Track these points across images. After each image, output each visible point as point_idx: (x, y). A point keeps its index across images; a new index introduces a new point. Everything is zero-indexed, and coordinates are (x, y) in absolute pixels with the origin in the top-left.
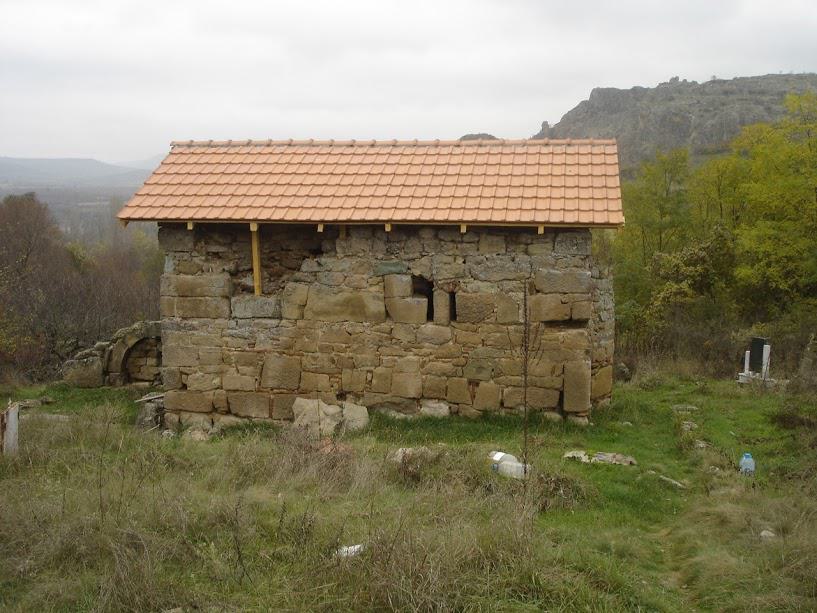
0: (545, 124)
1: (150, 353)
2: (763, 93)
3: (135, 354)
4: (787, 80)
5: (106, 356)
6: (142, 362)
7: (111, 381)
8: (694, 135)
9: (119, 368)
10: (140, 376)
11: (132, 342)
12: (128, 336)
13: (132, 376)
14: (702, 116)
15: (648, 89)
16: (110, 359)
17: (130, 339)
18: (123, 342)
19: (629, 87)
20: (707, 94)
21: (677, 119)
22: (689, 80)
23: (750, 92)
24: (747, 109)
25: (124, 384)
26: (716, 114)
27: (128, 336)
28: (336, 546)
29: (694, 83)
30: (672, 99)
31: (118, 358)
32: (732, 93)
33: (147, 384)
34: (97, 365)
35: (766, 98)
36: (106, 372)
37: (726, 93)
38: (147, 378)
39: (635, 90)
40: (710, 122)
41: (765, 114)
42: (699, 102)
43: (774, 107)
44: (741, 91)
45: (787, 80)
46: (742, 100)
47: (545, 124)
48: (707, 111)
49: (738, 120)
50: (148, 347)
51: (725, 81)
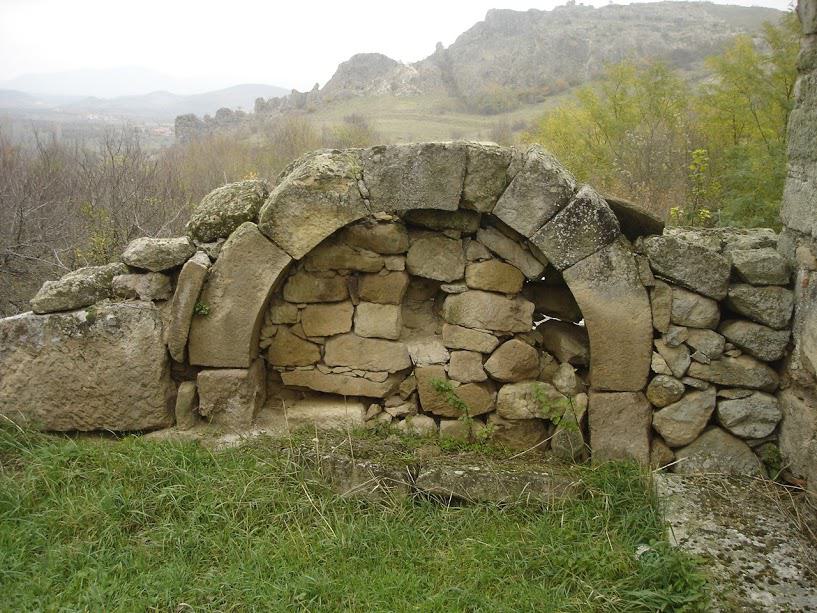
0: (439, 45)
1: (367, 285)
2: (659, 19)
3: (302, 288)
4: (683, 8)
5: (186, 293)
6: (335, 319)
7: (205, 406)
8: (591, 60)
9: (242, 350)
10: (323, 381)
11: (303, 237)
12: (295, 208)
13: (288, 379)
14: (599, 41)
15: (544, 12)
16: (198, 315)
17: (300, 221)
18: (268, 235)
19: (526, 10)
20: (604, 19)
21: (575, 43)
22: (586, 4)
23: (647, 18)
24: (643, 35)
25: (256, 419)
26: (612, 40)
27: (295, 208)
28: (112, 278)
29: (591, 7)
30: (569, 22)
31: (235, 306)
32: (628, 18)
33: (355, 411)
34: (140, 335)
35: (662, 25)
36: (180, 367)
37: (623, 18)
38: (356, 387)
39: (531, 12)
40: (608, 47)
41: (662, 40)
42: (595, 27)
43: (671, 34)
44: (638, 17)
45: (683, 8)
46: (639, 25)
47: (439, 45)
48: (604, 35)
49: (636, 46)
50: (368, 259)
51: (621, 7)
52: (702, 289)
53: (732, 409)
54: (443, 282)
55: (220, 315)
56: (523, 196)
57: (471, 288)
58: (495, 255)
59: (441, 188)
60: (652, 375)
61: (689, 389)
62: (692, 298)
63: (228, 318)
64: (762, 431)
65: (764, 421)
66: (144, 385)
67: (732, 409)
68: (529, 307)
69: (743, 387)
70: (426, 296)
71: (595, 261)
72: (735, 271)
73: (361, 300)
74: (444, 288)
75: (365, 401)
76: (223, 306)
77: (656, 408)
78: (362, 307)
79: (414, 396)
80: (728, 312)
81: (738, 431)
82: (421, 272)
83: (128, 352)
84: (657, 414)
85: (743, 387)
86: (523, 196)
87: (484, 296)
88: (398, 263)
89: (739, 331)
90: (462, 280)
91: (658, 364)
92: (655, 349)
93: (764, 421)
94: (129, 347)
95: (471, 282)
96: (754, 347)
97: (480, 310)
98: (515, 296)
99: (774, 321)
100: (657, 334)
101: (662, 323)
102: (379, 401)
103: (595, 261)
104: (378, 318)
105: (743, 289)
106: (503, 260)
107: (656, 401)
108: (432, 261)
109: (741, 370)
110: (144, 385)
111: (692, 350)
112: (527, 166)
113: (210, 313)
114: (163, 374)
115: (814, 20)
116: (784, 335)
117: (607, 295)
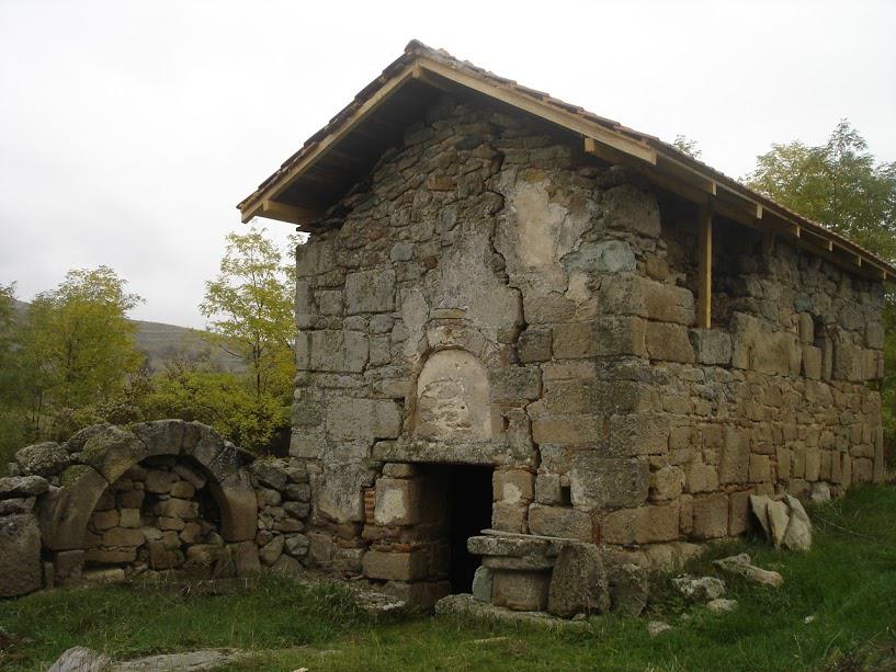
10: (105, 557)
12: (114, 456)
17: (115, 462)
33: (119, 572)
38: (121, 557)
52: (277, 487)
53: (291, 542)
54: (162, 494)
55: (70, 519)
56: (206, 446)
57: (172, 497)
58: (182, 479)
59: (174, 443)
60: (259, 530)
61: (275, 535)
62: (273, 491)
63: (76, 519)
64: (303, 551)
65: (303, 546)
66: (30, 565)
67: (291, 542)
68: (196, 505)
69: (294, 532)
70: (151, 507)
71: (234, 477)
72: (288, 477)
73: (124, 507)
74: (161, 497)
75: (122, 565)
76: (73, 512)
77: (260, 547)
78: (123, 511)
79: (148, 560)
80: (286, 497)
81: (294, 553)
82: (151, 489)
83: (22, 545)
84: (262, 550)
85: (294, 532)
86: (206, 446)
87: (179, 500)
88: (141, 485)
89: (291, 505)
90: (168, 493)
91: (261, 525)
92: (259, 518)
93: (303, 546)
94: (22, 542)
95: (173, 494)
96: (297, 512)
97: (177, 507)
98: (192, 500)
99: (305, 500)
100: (259, 510)
101: (262, 504)
102: (132, 565)
103: (234, 477)
104: (131, 516)
105: (292, 485)
106: (186, 481)
107: (262, 543)
108: (157, 483)
109: (293, 524)
110: (30, 565)
111: (273, 517)
112: (693, 330)
113: (67, 517)
114: (846, 292)
115: (450, 355)
116: (308, 504)
117: (238, 494)
